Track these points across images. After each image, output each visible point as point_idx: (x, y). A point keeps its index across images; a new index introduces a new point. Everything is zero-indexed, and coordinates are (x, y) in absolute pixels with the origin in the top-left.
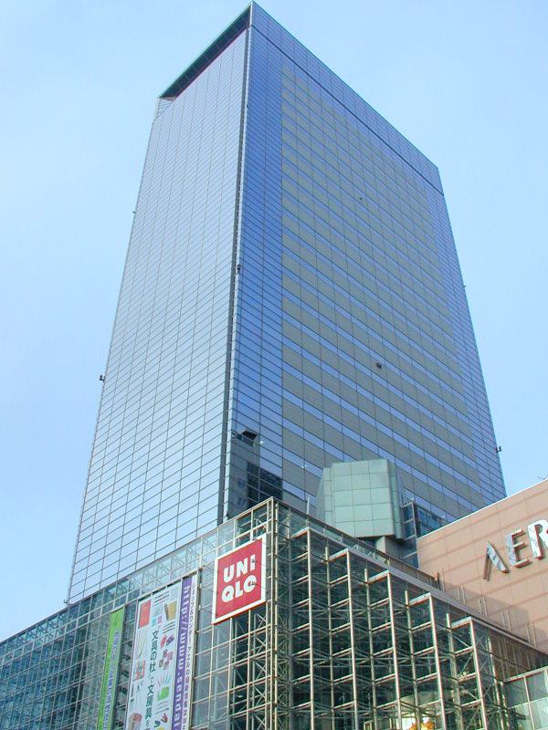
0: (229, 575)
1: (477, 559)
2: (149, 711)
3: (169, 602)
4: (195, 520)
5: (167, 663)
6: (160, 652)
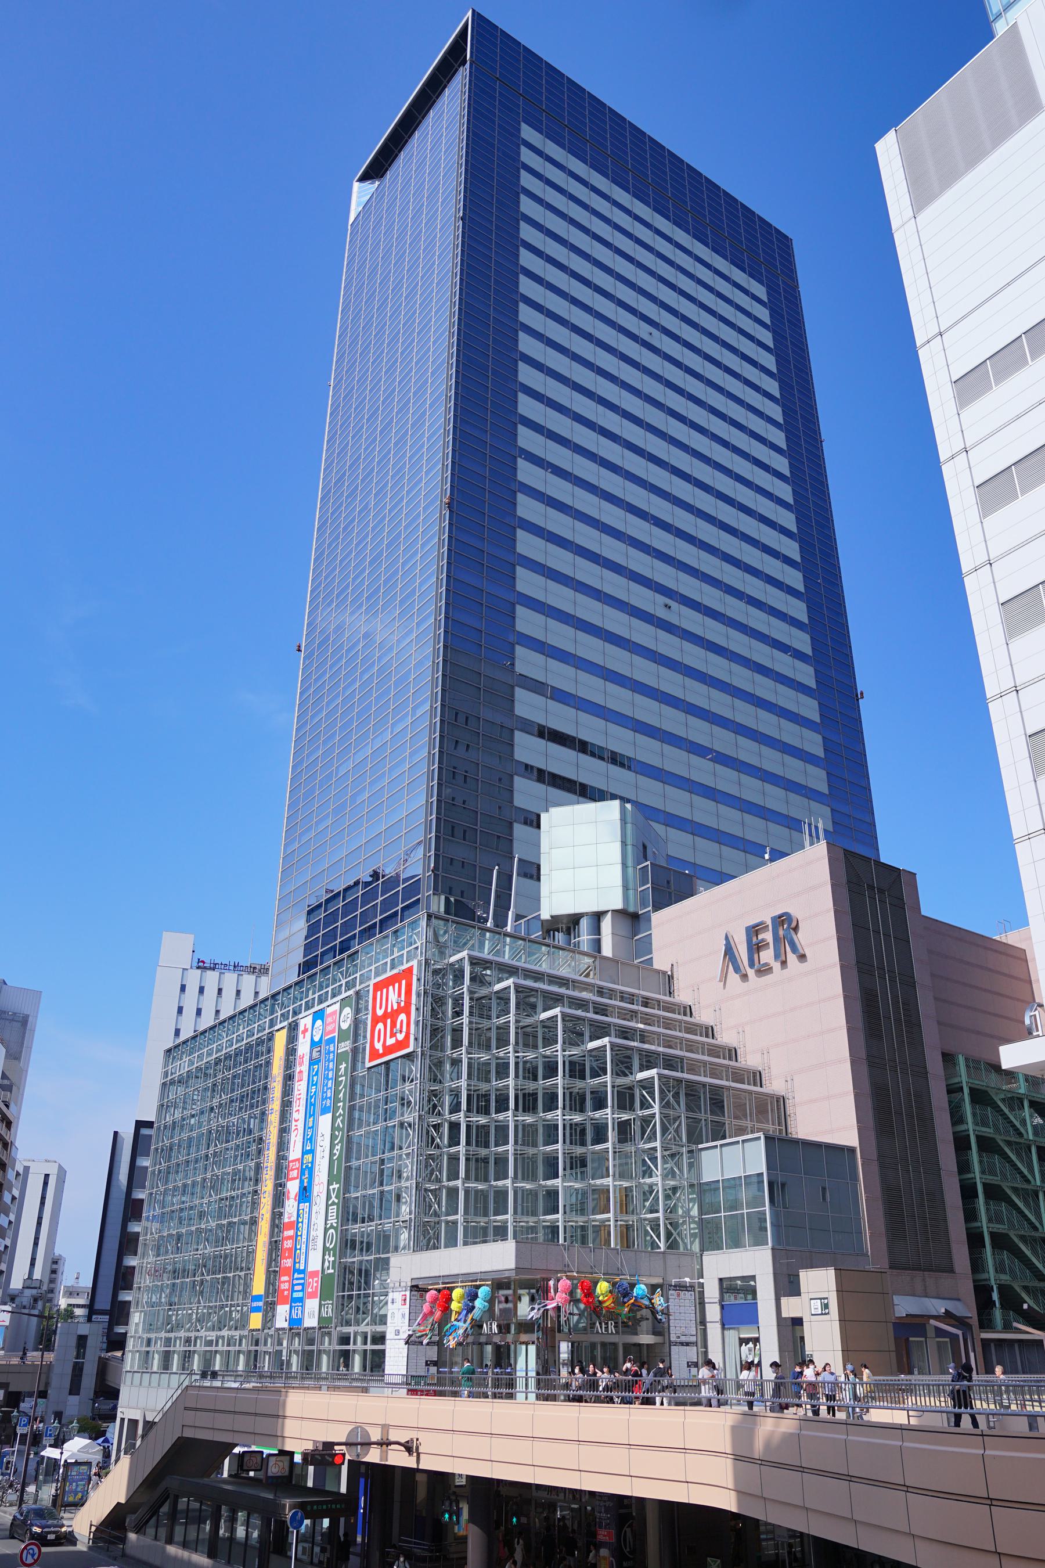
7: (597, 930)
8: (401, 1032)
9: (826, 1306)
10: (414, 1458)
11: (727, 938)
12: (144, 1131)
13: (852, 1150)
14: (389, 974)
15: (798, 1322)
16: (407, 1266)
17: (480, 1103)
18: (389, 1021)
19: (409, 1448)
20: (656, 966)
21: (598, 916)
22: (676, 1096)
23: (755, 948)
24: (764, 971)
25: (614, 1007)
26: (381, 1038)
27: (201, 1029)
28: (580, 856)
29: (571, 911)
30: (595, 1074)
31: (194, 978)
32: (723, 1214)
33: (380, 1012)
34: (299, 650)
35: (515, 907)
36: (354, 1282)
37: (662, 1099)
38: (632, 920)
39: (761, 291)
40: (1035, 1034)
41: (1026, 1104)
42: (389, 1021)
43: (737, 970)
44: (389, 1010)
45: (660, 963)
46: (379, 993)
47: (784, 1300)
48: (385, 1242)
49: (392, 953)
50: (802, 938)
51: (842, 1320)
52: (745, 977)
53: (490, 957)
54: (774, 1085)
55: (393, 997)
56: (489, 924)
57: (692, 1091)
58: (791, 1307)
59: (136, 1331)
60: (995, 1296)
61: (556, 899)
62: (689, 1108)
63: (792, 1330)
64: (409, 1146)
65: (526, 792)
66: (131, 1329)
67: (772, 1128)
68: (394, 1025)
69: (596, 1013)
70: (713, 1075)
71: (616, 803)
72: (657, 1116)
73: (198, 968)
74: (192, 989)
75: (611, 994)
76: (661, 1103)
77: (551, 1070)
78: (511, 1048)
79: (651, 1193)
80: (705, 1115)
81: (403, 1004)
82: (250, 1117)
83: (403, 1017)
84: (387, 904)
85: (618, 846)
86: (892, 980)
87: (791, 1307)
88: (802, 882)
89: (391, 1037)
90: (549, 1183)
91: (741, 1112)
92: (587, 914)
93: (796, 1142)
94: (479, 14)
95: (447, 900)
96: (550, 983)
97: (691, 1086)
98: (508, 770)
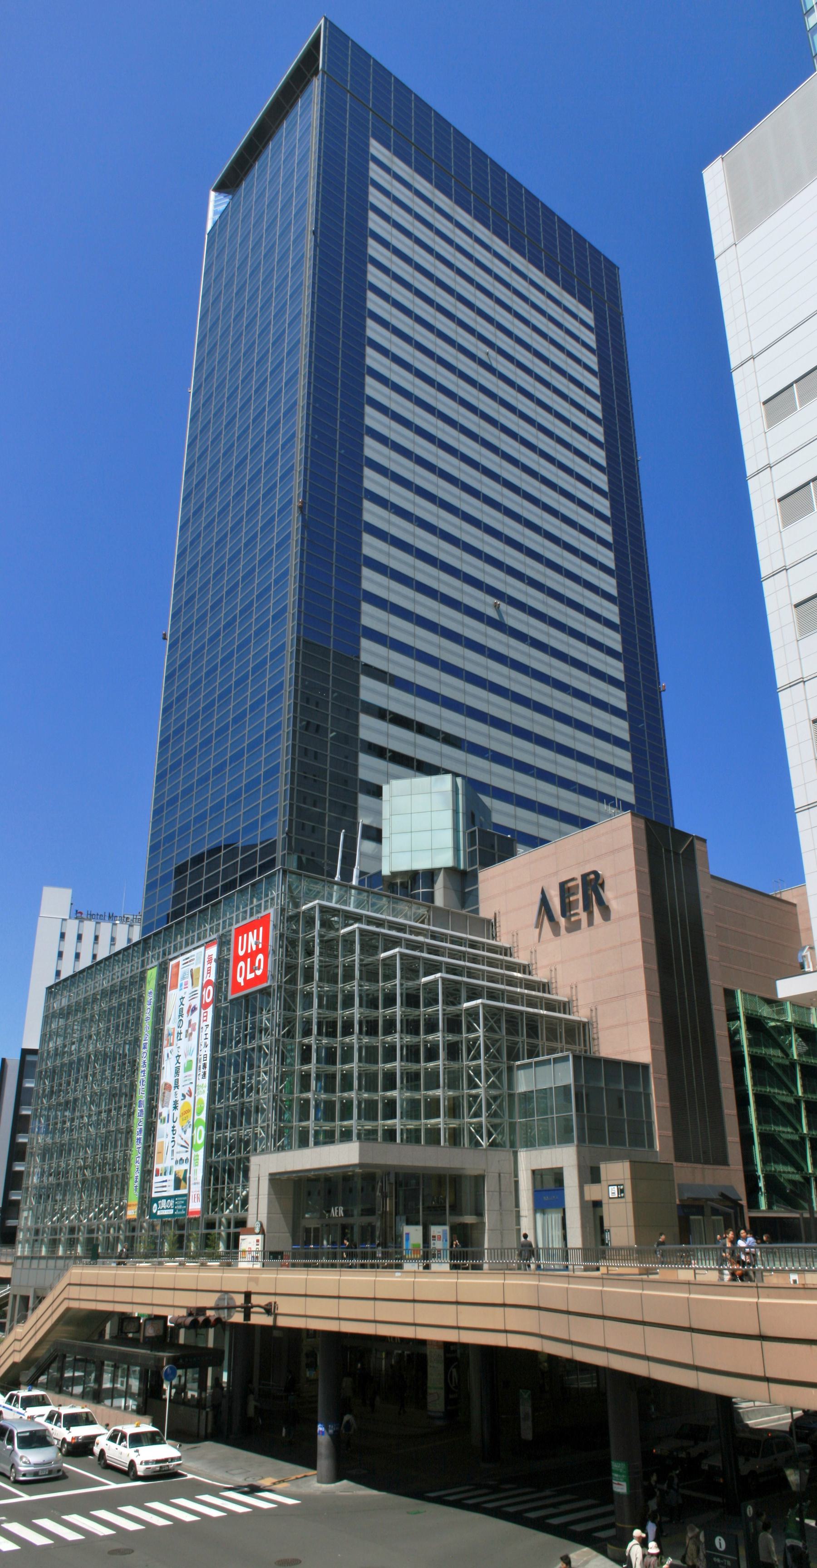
0: (260, 961)
1: (758, 472)
2: (177, 1081)
3: (193, 966)
4: (392, 178)
5: (191, 1034)
6: (185, 1019)
8: (259, 968)
9: (622, 1191)
11: (543, 892)
12: (29, 1058)
13: (645, 1067)
14: (248, 920)
15: (597, 1204)
16: (265, 1165)
17: (329, 1028)
18: (249, 960)
19: (269, 1310)
22: (498, 1022)
23: (567, 908)
24: (574, 927)
25: (445, 948)
26: (244, 974)
27: (78, 970)
28: (416, 824)
30: (428, 1004)
31: (72, 927)
33: (241, 953)
34: (165, 638)
35: (360, 864)
36: (225, 1171)
37: (485, 1025)
38: (463, 880)
39: (588, 316)
40: (807, 970)
41: (793, 1031)
42: (249, 960)
43: (551, 918)
44: (249, 951)
45: (486, 911)
46: (240, 938)
47: (587, 1188)
48: (246, 1145)
49: (252, 903)
50: (608, 895)
51: (635, 1202)
52: (556, 931)
53: (338, 906)
54: (580, 1015)
55: (252, 940)
56: (336, 879)
57: (513, 1018)
58: (593, 1192)
59: (26, 1224)
60: (761, 1184)
62: (509, 1032)
63: (594, 1211)
64: (267, 1065)
65: (369, 767)
66: (22, 1223)
67: (578, 1048)
68: (253, 963)
69: (430, 953)
70: (530, 1005)
71: (448, 778)
72: (482, 1039)
73: (76, 918)
74: (71, 937)
75: (442, 937)
76: (484, 1027)
77: (390, 1001)
78: (356, 983)
79: (475, 1101)
80: (523, 1039)
81: (260, 946)
82: (125, 1043)
83: (261, 956)
84: (245, 862)
85: (449, 814)
87: (593, 1192)
88: (611, 847)
89: (251, 972)
90: (389, 1094)
91: (552, 1034)
93: (598, 1060)
94: (331, 23)
95: (299, 859)
96: (390, 928)
97: (511, 1014)
98: (351, 745)
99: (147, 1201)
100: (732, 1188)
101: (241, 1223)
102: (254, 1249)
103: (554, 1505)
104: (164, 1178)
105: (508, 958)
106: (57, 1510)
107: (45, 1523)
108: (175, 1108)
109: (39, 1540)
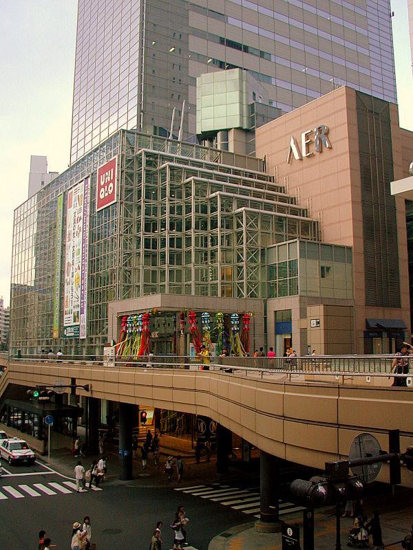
6: (76, 225)
7: (226, 138)
9: (318, 323)
10: (90, 392)
13: (350, 248)
16: (116, 307)
19: (86, 388)
20: (257, 157)
21: (227, 130)
22: (256, 221)
29: (212, 129)
32: (288, 278)
54: (314, 217)
61: (204, 123)
86: (380, 162)
92: (221, 130)
96: (193, 165)
99: (62, 328)
100: (402, 322)
101: (105, 339)
102: (110, 355)
103: (242, 499)
104: (68, 316)
105: (271, 183)
106: (30, 482)
107: (39, 486)
108: (73, 276)
109: (34, 494)
